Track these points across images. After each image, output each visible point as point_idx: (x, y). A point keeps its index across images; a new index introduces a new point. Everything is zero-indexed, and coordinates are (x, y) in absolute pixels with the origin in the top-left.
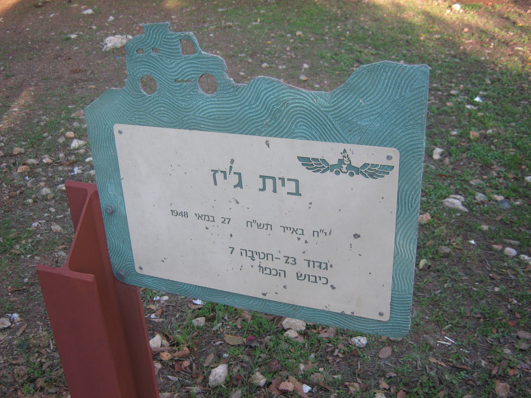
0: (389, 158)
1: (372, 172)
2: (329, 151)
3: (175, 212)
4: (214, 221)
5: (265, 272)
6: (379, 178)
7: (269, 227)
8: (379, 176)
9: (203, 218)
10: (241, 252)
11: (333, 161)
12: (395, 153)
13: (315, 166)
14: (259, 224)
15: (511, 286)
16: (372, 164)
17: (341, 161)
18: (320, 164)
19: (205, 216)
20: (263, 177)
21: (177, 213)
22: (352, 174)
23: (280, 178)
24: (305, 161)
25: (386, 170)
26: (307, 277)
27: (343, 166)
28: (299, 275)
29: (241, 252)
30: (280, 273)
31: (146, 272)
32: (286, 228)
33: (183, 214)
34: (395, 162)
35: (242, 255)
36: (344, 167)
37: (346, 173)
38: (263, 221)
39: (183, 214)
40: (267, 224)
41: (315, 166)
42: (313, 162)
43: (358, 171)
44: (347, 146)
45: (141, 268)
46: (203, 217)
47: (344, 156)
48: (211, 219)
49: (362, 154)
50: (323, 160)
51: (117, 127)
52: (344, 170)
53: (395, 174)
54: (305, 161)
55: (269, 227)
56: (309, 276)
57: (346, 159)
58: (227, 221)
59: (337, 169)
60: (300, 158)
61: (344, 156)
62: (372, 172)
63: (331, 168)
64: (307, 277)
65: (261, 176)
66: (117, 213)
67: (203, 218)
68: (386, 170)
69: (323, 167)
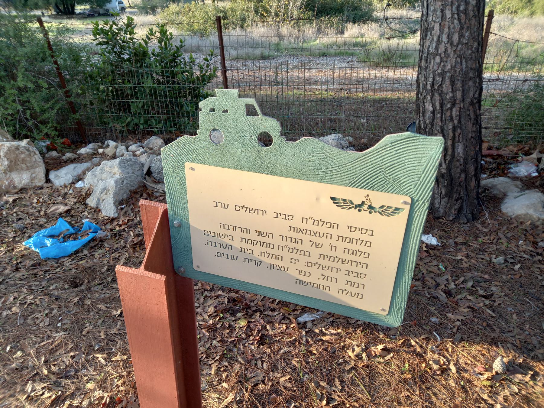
0: (405, 203)
2: (357, 195)
4: (309, 256)
9: (304, 232)
11: (357, 202)
12: (409, 201)
13: (343, 204)
18: (347, 203)
22: (370, 213)
31: (202, 269)
34: (408, 207)
36: (365, 207)
41: (343, 204)
42: (342, 202)
44: (370, 192)
45: (198, 267)
46: (305, 231)
48: (307, 254)
49: (378, 198)
53: (403, 216)
57: (368, 201)
59: (359, 207)
60: (332, 198)
62: (385, 211)
63: (356, 207)
67: (304, 232)
69: (349, 205)
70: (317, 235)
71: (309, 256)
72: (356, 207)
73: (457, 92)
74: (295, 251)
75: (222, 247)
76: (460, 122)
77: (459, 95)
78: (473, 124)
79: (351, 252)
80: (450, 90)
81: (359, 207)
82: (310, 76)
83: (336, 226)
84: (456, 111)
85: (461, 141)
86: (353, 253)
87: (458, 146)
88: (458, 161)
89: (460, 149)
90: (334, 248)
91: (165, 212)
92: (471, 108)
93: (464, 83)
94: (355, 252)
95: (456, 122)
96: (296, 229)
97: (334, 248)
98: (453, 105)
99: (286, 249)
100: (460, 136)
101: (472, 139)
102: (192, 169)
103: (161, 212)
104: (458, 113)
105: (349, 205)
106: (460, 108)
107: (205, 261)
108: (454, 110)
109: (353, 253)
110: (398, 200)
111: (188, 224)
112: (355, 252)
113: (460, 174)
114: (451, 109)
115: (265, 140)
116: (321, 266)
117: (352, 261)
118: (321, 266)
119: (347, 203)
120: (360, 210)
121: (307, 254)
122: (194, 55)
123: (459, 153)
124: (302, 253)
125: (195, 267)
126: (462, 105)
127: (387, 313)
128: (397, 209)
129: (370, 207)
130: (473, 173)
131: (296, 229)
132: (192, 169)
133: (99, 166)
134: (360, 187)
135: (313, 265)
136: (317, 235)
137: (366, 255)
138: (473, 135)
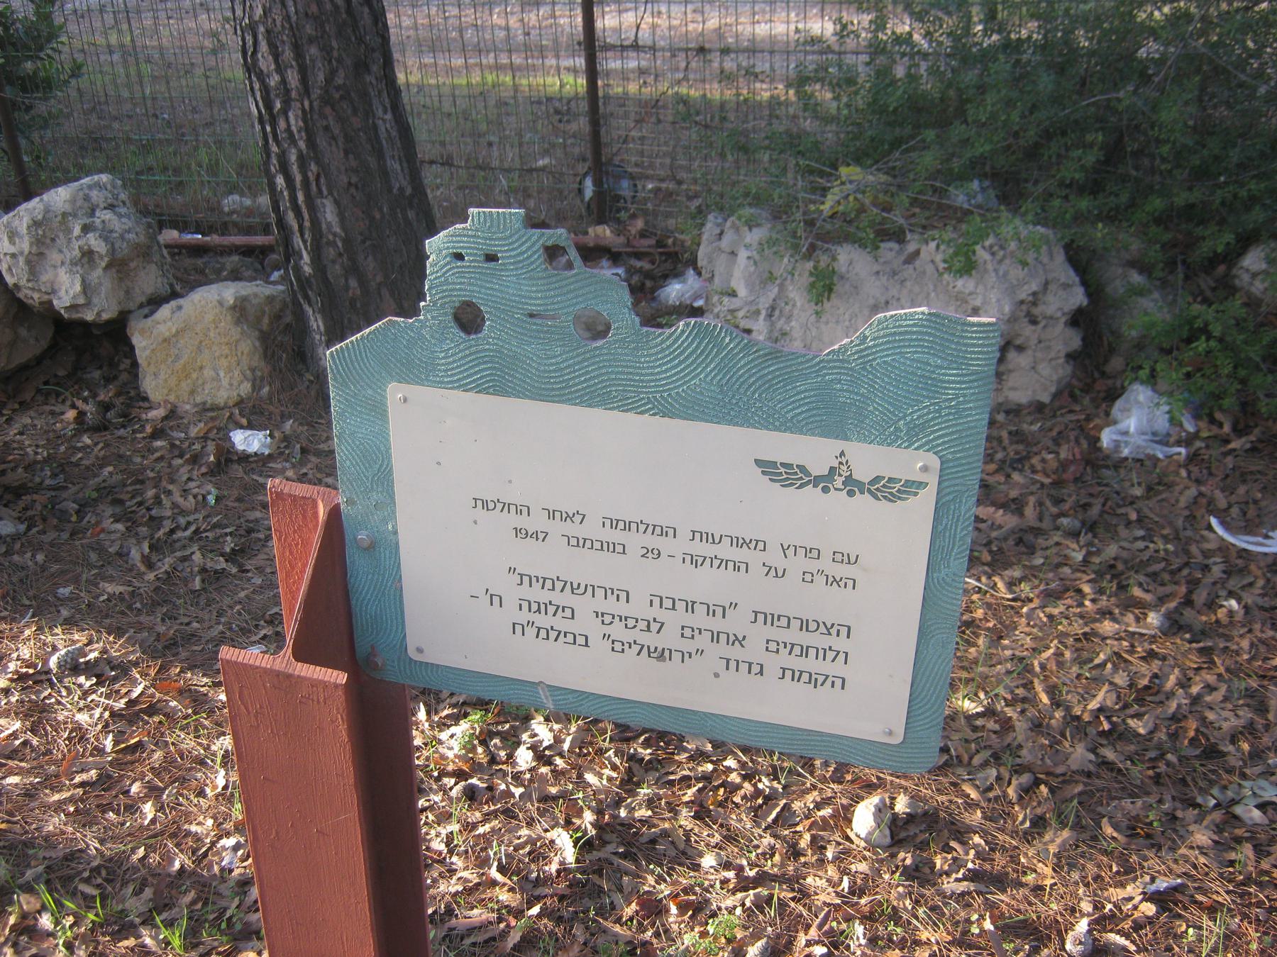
2: (816, 452)
4: (587, 645)
5: (776, 622)
8: (900, 498)
9: (752, 545)
11: (819, 469)
12: (935, 462)
14: (575, 586)
15: (1185, 572)
16: (907, 481)
18: (796, 473)
19: (655, 526)
22: (851, 494)
24: (767, 467)
25: (911, 487)
26: (590, 589)
31: (431, 657)
32: (687, 656)
34: (933, 480)
36: (839, 482)
42: (782, 470)
43: (861, 487)
45: (420, 650)
46: (754, 543)
47: (841, 463)
48: (581, 640)
49: (868, 459)
50: (802, 468)
54: (767, 467)
58: (541, 536)
59: (824, 482)
60: (758, 462)
61: (841, 463)
62: (887, 490)
63: (816, 481)
64: (590, 589)
66: (384, 550)
67: (752, 545)
68: (911, 487)
69: (801, 478)
71: (587, 645)
72: (816, 481)
73: (289, 72)
74: (553, 635)
75: (710, 540)
76: (311, 143)
77: (293, 78)
78: (346, 153)
79: (534, 607)
80: (273, 67)
83: (671, 532)
84: (296, 117)
85: (325, 192)
86: (539, 610)
87: (324, 206)
88: (329, 243)
89: (329, 214)
90: (496, 600)
92: (328, 110)
93: (299, 55)
94: (543, 607)
95: (302, 144)
97: (496, 600)
98: (287, 103)
99: (531, 632)
100: (322, 180)
101: (353, 190)
104: (301, 123)
105: (801, 478)
106: (304, 110)
108: (291, 114)
109: (539, 610)
110: (916, 463)
112: (543, 607)
113: (347, 280)
114: (285, 111)
116: (645, 649)
118: (645, 649)
119: (796, 473)
121: (581, 640)
123: (329, 225)
124: (570, 638)
125: (412, 653)
126: (306, 103)
129: (849, 480)
130: (379, 278)
135: (627, 646)
137: (568, 613)
138: (354, 180)
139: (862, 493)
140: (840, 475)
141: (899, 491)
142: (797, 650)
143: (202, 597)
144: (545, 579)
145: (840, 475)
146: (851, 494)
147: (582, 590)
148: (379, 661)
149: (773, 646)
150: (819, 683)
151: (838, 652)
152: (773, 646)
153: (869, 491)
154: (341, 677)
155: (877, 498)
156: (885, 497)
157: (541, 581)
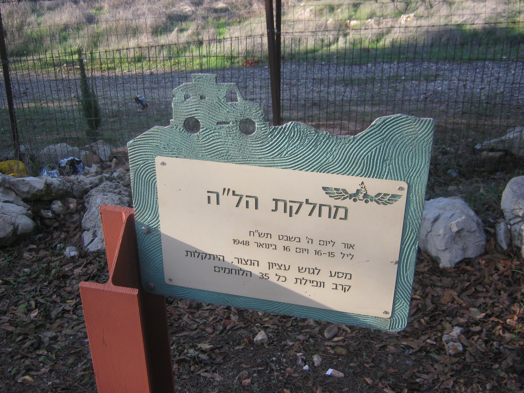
0: (401, 189)
1: (383, 199)
2: (350, 183)
3: (237, 241)
6: (388, 205)
7: (269, 236)
8: (388, 203)
10: (209, 197)
12: (405, 185)
13: (337, 194)
17: (358, 190)
20: (276, 201)
21: (239, 242)
23: (335, 206)
26: (307, 270)
27: (361, 195)
28: (301, 268)
29: (209, 197)
30: (247, 202)
31: (175, 283)
33: (245, 243)
34: (404, 193)
35: (209, 202)
36: (361, 196)
37: (362, 200)
38: (263, 231)
39: (245, 243)
40: (267, 234)
41: (337, 194)
42: (335, 192)
45: (171, 280)
49: (375, 185)
50: (344, 190)
51: (159, 160)
52: (361, 198)
53: (402, 202)
55: (269, 236)
56: (309, 269)
59: (354, 197)
60: (324, 188)
62: (383, 199)
63: (351, 196)
64: (307, 270)
65: (274, 200)
70: (283, 268)
72: (351, 196)
81: (354, 197)
82: (36, 107)
91: (131, 220)
96: (346, 245)
102: (163, 164)
103: (124, 218)
107: (178, 274)
111: (157, 230)
115: (246, 127)
117: (309, 269)
120: (355, 200)
122: (22, 92)
127: (390, 315)
128: (393, 196)
129: (366, 195)
131: (346, 245)
132: (163, 164)
133: (432, 302)
134: (348, 173)
136: (283, 268)
137: (297, 240)
139: (371, 201)
140: (361, 193)
141: (389, 200)
142: (227, 271)
143: (39, 285)
144: (225, 269)
145: (361, 193)
146: (366, 202)
147: (293, 239)
148: (152, 285)
149: (217, 269)
150: (346, 290)
151: (307, 280)
152: (217, 269)
153: (375, 201)
154: (136, 292)
155: (379, 204)
156: (383, 204)
157: (224, 269)
